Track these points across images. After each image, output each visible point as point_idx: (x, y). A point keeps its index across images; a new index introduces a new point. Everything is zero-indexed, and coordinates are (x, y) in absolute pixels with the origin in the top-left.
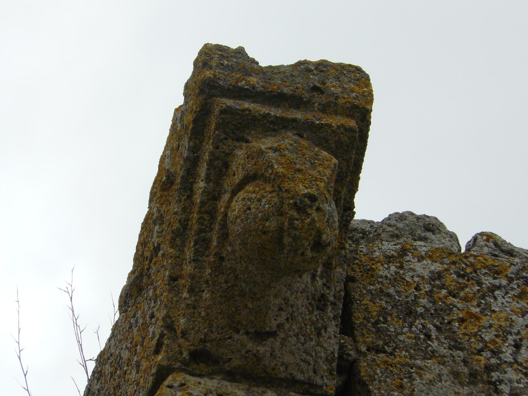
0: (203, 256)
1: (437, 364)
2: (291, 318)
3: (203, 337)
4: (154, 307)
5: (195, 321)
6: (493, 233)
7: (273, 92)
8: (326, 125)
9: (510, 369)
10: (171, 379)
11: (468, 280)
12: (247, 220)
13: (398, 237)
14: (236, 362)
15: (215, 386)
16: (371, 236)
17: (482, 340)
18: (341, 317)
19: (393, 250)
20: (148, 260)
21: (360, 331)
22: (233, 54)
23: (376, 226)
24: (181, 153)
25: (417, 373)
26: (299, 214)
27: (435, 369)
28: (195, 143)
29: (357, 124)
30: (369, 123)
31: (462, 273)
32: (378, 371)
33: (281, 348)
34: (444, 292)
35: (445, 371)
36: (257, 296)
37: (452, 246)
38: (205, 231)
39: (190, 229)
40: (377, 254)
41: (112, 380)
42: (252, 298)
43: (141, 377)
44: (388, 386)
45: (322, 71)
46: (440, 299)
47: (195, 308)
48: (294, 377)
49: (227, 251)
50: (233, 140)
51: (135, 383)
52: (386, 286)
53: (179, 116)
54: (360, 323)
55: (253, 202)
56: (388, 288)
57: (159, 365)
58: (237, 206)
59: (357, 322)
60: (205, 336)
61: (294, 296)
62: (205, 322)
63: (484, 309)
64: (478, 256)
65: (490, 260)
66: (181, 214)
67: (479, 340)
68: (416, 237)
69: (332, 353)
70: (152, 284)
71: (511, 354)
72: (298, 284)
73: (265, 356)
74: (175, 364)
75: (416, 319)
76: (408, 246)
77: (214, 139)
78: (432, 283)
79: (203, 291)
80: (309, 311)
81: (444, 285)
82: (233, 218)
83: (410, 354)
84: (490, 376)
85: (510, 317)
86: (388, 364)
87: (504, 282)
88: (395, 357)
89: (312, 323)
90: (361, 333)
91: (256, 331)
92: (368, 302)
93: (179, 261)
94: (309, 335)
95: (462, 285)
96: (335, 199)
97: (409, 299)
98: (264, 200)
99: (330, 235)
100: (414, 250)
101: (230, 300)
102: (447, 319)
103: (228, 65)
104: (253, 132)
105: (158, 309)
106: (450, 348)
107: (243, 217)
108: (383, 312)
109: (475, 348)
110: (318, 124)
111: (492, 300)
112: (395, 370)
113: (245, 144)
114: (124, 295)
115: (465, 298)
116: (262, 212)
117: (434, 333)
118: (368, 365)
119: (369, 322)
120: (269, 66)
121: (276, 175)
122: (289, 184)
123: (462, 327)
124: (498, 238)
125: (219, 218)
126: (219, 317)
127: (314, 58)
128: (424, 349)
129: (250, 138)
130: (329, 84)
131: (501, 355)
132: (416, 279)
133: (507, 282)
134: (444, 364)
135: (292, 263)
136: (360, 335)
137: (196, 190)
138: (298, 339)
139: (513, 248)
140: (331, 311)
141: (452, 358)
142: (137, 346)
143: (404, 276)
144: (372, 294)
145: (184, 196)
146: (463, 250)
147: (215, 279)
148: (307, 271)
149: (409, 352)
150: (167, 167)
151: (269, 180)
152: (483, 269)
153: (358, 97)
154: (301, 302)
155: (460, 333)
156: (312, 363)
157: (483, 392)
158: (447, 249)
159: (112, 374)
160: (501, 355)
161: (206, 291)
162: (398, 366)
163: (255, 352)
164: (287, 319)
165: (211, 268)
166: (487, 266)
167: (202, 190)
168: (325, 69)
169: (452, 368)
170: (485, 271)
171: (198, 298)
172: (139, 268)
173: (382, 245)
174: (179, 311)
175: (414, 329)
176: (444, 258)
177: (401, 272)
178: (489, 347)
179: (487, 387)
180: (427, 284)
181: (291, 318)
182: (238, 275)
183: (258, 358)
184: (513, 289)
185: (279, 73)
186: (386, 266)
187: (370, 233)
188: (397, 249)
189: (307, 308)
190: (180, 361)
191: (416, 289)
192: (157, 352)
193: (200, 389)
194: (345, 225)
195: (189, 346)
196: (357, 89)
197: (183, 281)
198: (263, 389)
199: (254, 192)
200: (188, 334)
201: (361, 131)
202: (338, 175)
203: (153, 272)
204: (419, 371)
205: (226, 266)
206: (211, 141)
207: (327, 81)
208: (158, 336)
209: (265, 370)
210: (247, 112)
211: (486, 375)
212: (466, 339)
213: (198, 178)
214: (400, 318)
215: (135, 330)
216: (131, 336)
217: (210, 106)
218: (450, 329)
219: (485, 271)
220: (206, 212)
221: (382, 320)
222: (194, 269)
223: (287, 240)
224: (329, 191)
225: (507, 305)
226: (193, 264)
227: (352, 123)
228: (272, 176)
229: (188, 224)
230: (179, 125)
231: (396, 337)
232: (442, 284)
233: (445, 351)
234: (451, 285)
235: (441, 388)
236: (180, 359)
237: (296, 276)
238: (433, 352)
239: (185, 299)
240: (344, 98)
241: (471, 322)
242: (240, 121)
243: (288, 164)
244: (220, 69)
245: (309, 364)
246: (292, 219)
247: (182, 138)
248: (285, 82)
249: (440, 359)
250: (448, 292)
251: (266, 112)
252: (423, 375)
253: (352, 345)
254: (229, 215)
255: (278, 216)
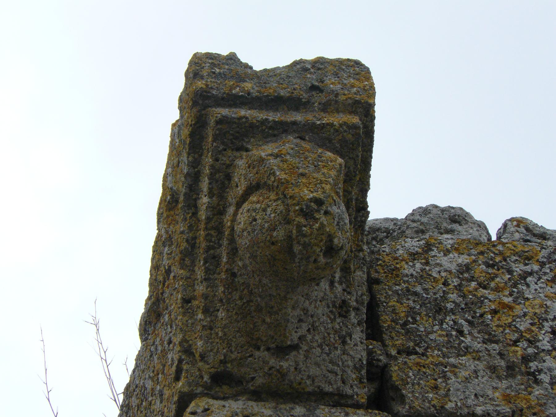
0: (214, 274)
1: (472, 360)
2: (313, 328)
3: (223, 358)
4: (171, 332)
5: (212, 343)
6: (523, 218)
7: (270, 96)
8: (328, 124)
9: (548, 357)
10: (194, 405)
11: (498, 270)
12: (254, 232)
13: (423, 232)
14: (260, 381)
15: (240, 407)
16: (395, 234)
17: (517, 330)
18: (366, 322)
19: (417, 247)
20: (162, 284)
21: (389, 334)
22: (224, 61)
23: (399, 223)
24: (181, 169)
25: (451, 371)
26: (306, 220)
27: (470, 366)
28: (194, 157)
29: (360, 120)
30: (373, 118)
31: (491, 262)
32: (411, 374)
33: (305, 361)
34: (473, 284)
35: (481, 366)
36: (274, 310)
37: (480, 236)
38: (213, 248)
39: (199, 247)
40: (401, 252)
41: (139, 412)
42: (269, 312)
43: (165, 406)
44: (422, 388)
45: (319, 69)
46: (470, 292)
47: (211, 328)
48: (322, 390)
49: (239, 266)
50: (233, 150)
51: (160, 413)
52: (413, 284)
53: (176, 131)
54: (388, 326)
55: (258, 212)
56: (414, 286)
57: (179, 392)
58: (242, 219)
59: (385, 325)
60: (225, 357)
61: (313, 306)
62: (223, 342)
63: (517, 298)
64: (507, 243)
65: (519, 246)
66: (188, 233)
67: (514, 331)
68: (442, 231)
69: (360, 360)
70: (167, 309)
71: (548, 342)
72: (316, 293)
73: (289, 371)
74: (196, 389)
75: (446, 316)
76: (433, 241)
77: (213, 151)
78: (461, 276)
79: (218, 310)
80: (330, 319)
81: (473, 277)
82: (240, 232)
83: (442, 353)
84: (528, 366)
85: (545, 303)
86: (420, 366)
87: (536, 267)
88: (428, 358)
89: (336, 331)
90: (390, 336)
91: (277, 346)
92: (394, 303)
93: (190, 281)
94: (334, 344)
95: (492, 275)
96: (346, 200)
97: (438, 296)
98: (269, 210)
99: (343, 238)
100: (439, 244)
101: (246, 317)
102: (479, 312)
103: (220, 73)
104: (252, 140)
105: (174, 334)
106: (484, 342)
107: (249, 229)
108: (412, 312)
109: (510, 340)
110: (319, 125)
111: (524, 288)
112: (428, 371)
113: (245, 153)
114: (143, 323)
115: (496, 288)
116: (268, 222)
117: (466, 329)
118: (400, 369)
119: (397, 324)
120: (264, 69)
121: (279, 182)
122: (293, 190)
123: (495, 319)
124: (529, 222)
125: (226, 233)
126: (237, 335)
127: (310, 56)
128: (456, 345)
129: (249, 147)
130: (327, 81)
131: (538, 344)
132: (443, 274)
133: (539, 267)
134: (479, 359)
135: (305, 272)
136: (389, 339)
137: (200, 206)
138: (322, 350)
139: (545, 231)
140: (355, 317)
141: (487, 352)
142: (158, 374)
143: (430, 273)
144: (398, 294)
145: (189, 213)
146: (494, 238)
147: (229, 296)
148: (322, 278)
149: (442, 351)
150: (170, 186)
151: (273, 188)
152: (512, 257)
153: (358, 92)
154: (321, 311)
155: (493, 325)
156: (340, 373)
157: (522, 384)
158: (475, 239)
159: (139, 406)
160: (537, 344)
161: (221, 310)
162: (431, 366)
163: (278, 368)
164: (309, 330)
165: (224, 286)
166: (517, 253)
167: (206, 205)
168: (323, 66)
169: (488, 362)
170: (515, 258)
171: (213, 318)
172: (155, 294)
173: (406, 242)
174: (195, 334)
175: (445, 326)
176: (471, 249)
177: (427, 268)
178: (525, 336)
179: (526, 378)
180: (455, 278)
181: (313, 328)
182: (252, 290)
183: (282, 375)
184: (545, 274)
185: (275, 75)
186: (411, 264)
187: (395, 231)
188: (421, 245)
189: (329, 316)
190: (201, 386)
191: (444, 284)
192: (177, 378)
193: (225, 412)
194: (360, 226)
195: (209, 369)
196: (357, 83)
197: (197, 302)
198: (291, 406)
199: (258, 202)
200: (207, 357)
201: (365, 127)
202: (346, 175)
203: (166, 295)
204: (453, 369)
205: (239, 282)
206: (210, 154)
207: (325, 78)
208: (177, 362)
209: (290, 386)
210: (244, 120)
211: (524, 366)
212: (500, 331)
213: (201, 193)
214: (430, 317)
215: (156, 357)
216: (152, 365)
217: (206, 118)
218: (483, 322)
219: (515, 258)
220: (213, 228)
221: (411, 320)
222: (207, 288)
223: (297, 248)
224: (337, 193)
225: (541, 291)
226: (205, 284)
227: (355, 120)
228: (275, 184)
229: (195, 243)
230: (177, 141)
231: (427, 336)
232: (471, 276)
233: (479, 345)
234: (481, 276)
235: (478, 385)
236: (202, 384)
237: (313, 284)
238: (467, 348)
239: (200, 321)
240: (344, 95)
241: (504, 312)
242: (238, 129)
243: (291, 169)
244: (212, 78)
245: (337, 374)
246: (299, 226)
247: (181, 154)
248: (282, 84)
249: (475, 355)
250: (478, 284)
251: (264, 118)
252: (458, 374)
253: (381, 350)
254: (236, 228)
255: (285, 224)
